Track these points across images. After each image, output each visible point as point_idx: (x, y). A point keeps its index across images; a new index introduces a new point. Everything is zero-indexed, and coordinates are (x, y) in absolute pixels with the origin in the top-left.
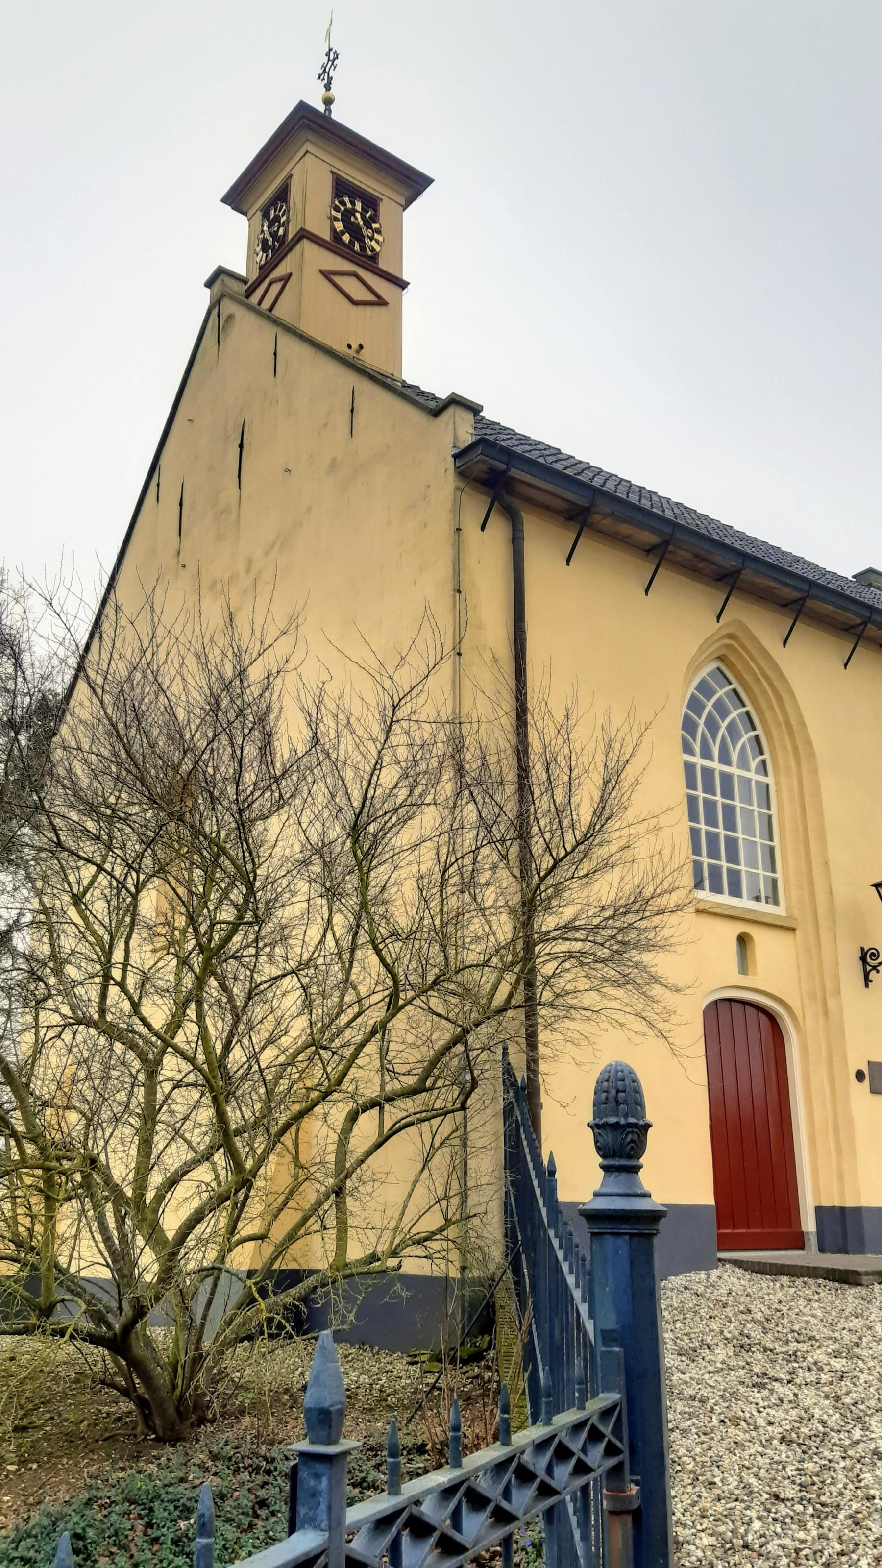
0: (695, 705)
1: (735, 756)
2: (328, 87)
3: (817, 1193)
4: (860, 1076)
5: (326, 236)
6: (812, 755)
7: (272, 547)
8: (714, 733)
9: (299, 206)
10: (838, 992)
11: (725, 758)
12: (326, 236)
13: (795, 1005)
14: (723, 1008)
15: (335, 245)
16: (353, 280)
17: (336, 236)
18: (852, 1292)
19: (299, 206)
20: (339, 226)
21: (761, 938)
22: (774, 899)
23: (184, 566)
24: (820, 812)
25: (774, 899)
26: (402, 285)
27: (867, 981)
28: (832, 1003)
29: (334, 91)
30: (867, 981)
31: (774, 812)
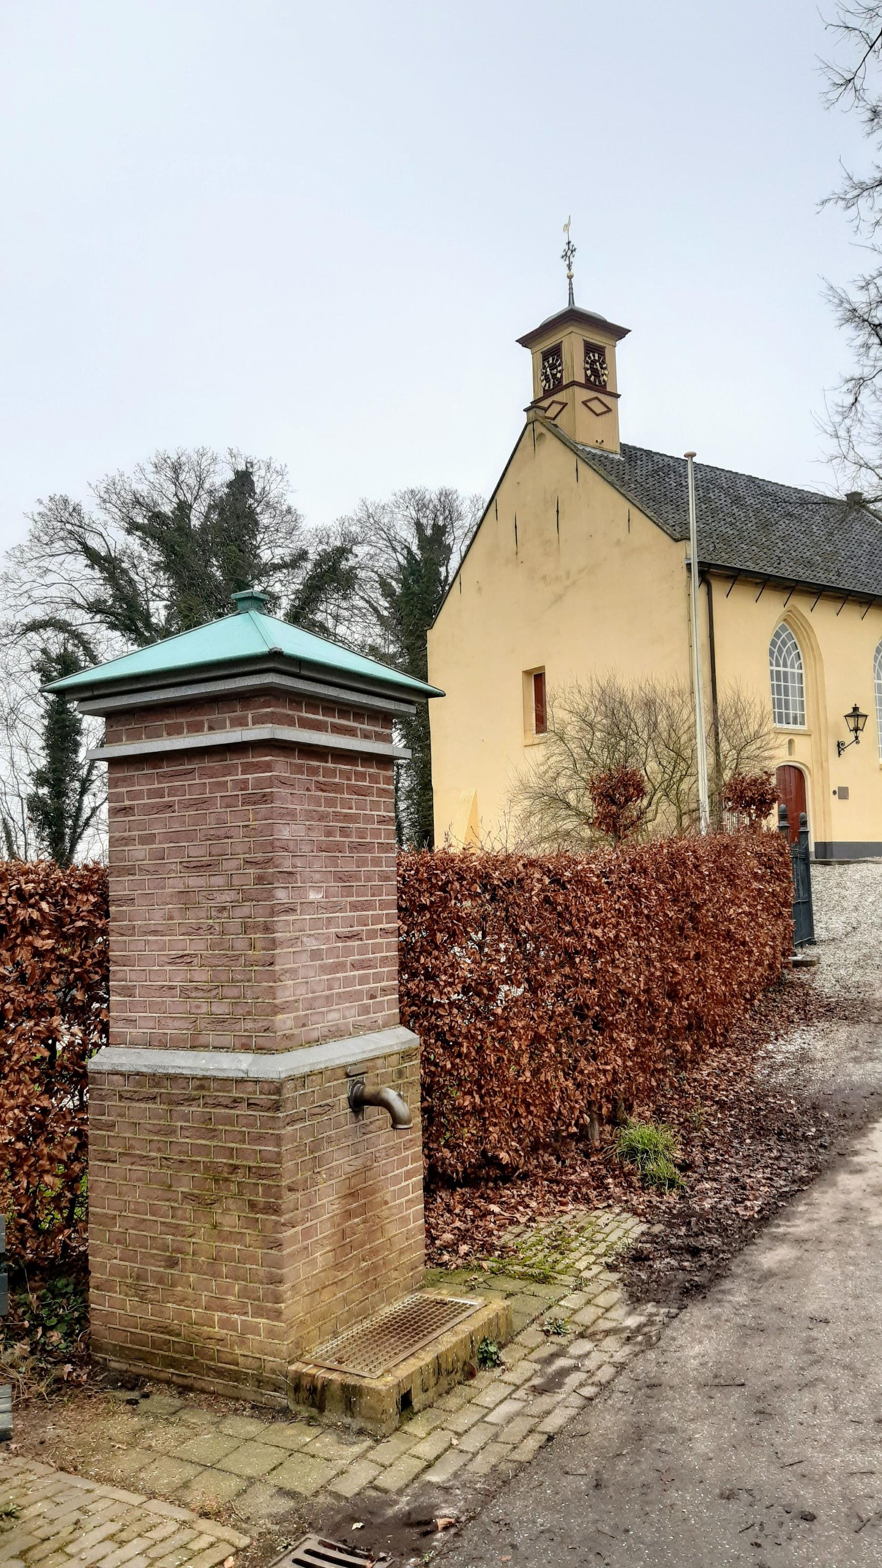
0: (773, 644)
1: (789, 663)
2: (569, 266)
3: (816, 837)
4: (834, 792)
5: (583, 381)
6: (821, 660)
7: (583, 570)
8: (780, 654)
9: (569, 362)
10: (827, 761)
11: (785, 666)
12: (583, 381)
13: (810, 767)
14: (787, 769)
15: (588, 385)
16: (596, 402)
17: (587, 378)
18: (828, 868)
19: (569, 362)
20: (589, 372)
21: (797, 740)
22: (802, 723)
23: (843, 793)
24: (824, 685)
25: (802, 723)
26: (618, 396)
27: (839, 754)
28: (825, 764)
29: (574, 270)
30: (839, 754)
31: (804, 685)
